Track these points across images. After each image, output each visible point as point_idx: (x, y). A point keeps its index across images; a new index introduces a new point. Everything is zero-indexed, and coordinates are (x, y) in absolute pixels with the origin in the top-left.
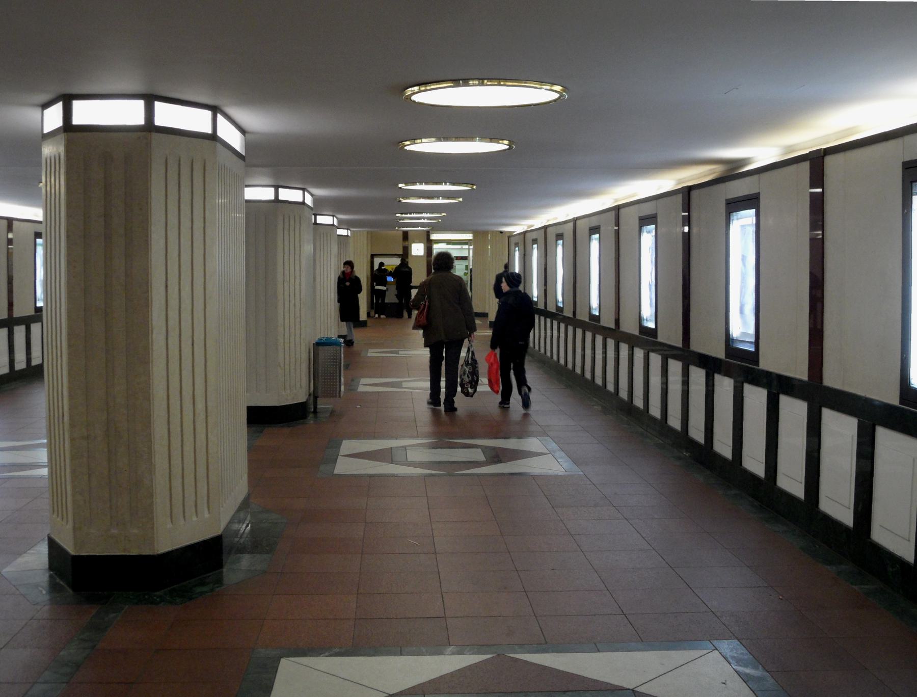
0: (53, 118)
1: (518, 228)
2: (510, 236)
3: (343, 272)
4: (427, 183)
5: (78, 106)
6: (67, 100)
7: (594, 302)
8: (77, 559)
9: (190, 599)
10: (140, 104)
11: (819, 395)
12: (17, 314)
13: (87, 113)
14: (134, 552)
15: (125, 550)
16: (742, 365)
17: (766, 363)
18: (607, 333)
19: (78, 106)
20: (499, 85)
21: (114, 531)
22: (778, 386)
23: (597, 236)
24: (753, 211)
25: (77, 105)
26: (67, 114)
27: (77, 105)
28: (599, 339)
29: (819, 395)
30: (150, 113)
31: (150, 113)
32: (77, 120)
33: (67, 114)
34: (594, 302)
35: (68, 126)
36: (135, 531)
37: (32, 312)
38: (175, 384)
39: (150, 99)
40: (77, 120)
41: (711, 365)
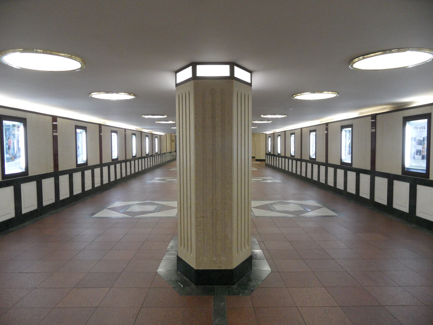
0: (187, 74)
1: (268, 133)
2: (266, 135)
3: (372, 132)
4: (259, 121)
5: (199, 68)
6: (194, 65)
7: (270, 150)
8: (198, 271)
9: (252, 291)
10: (227, 67)
11: (327, 165)
12: (127, 158)
13: (203, 71)
14: (223, 268)
15: (219, 267)
16: (313, 161)
17: (317, 160)
18: (272, 155)
19: (199, 68)
20: (364, 58)
21: (215, 259)
22: (319, 164)
23: (133, 155)
24: (78, 163)
25: (198, 67)
26: (194, 71)
27: (198, 67)
28: (270, 156)
29: (327, 165)
30: (232, 71)
31: (232, 71)
32: (199, 74)
33: (194, 71)
34: (270, 150)
35: (194, 77)
36: (224, 258)
37: (111, 161)
38: (239, 193)
39: (232, 65)
40: (199, 74)
41: (289, 158)
